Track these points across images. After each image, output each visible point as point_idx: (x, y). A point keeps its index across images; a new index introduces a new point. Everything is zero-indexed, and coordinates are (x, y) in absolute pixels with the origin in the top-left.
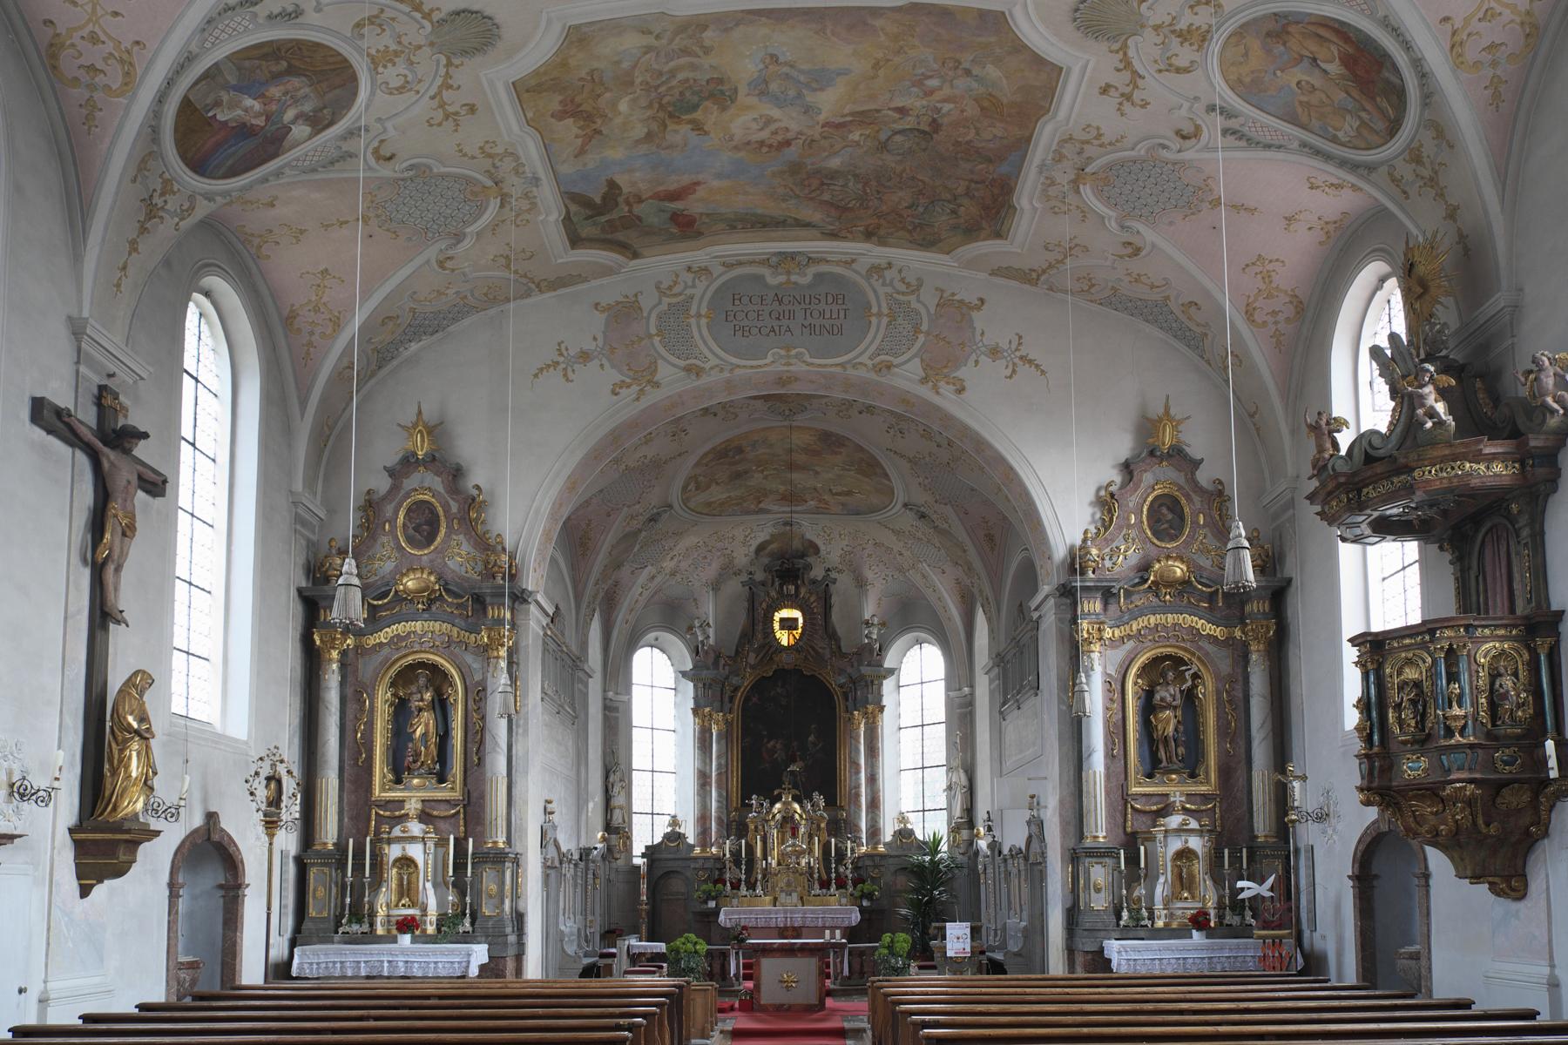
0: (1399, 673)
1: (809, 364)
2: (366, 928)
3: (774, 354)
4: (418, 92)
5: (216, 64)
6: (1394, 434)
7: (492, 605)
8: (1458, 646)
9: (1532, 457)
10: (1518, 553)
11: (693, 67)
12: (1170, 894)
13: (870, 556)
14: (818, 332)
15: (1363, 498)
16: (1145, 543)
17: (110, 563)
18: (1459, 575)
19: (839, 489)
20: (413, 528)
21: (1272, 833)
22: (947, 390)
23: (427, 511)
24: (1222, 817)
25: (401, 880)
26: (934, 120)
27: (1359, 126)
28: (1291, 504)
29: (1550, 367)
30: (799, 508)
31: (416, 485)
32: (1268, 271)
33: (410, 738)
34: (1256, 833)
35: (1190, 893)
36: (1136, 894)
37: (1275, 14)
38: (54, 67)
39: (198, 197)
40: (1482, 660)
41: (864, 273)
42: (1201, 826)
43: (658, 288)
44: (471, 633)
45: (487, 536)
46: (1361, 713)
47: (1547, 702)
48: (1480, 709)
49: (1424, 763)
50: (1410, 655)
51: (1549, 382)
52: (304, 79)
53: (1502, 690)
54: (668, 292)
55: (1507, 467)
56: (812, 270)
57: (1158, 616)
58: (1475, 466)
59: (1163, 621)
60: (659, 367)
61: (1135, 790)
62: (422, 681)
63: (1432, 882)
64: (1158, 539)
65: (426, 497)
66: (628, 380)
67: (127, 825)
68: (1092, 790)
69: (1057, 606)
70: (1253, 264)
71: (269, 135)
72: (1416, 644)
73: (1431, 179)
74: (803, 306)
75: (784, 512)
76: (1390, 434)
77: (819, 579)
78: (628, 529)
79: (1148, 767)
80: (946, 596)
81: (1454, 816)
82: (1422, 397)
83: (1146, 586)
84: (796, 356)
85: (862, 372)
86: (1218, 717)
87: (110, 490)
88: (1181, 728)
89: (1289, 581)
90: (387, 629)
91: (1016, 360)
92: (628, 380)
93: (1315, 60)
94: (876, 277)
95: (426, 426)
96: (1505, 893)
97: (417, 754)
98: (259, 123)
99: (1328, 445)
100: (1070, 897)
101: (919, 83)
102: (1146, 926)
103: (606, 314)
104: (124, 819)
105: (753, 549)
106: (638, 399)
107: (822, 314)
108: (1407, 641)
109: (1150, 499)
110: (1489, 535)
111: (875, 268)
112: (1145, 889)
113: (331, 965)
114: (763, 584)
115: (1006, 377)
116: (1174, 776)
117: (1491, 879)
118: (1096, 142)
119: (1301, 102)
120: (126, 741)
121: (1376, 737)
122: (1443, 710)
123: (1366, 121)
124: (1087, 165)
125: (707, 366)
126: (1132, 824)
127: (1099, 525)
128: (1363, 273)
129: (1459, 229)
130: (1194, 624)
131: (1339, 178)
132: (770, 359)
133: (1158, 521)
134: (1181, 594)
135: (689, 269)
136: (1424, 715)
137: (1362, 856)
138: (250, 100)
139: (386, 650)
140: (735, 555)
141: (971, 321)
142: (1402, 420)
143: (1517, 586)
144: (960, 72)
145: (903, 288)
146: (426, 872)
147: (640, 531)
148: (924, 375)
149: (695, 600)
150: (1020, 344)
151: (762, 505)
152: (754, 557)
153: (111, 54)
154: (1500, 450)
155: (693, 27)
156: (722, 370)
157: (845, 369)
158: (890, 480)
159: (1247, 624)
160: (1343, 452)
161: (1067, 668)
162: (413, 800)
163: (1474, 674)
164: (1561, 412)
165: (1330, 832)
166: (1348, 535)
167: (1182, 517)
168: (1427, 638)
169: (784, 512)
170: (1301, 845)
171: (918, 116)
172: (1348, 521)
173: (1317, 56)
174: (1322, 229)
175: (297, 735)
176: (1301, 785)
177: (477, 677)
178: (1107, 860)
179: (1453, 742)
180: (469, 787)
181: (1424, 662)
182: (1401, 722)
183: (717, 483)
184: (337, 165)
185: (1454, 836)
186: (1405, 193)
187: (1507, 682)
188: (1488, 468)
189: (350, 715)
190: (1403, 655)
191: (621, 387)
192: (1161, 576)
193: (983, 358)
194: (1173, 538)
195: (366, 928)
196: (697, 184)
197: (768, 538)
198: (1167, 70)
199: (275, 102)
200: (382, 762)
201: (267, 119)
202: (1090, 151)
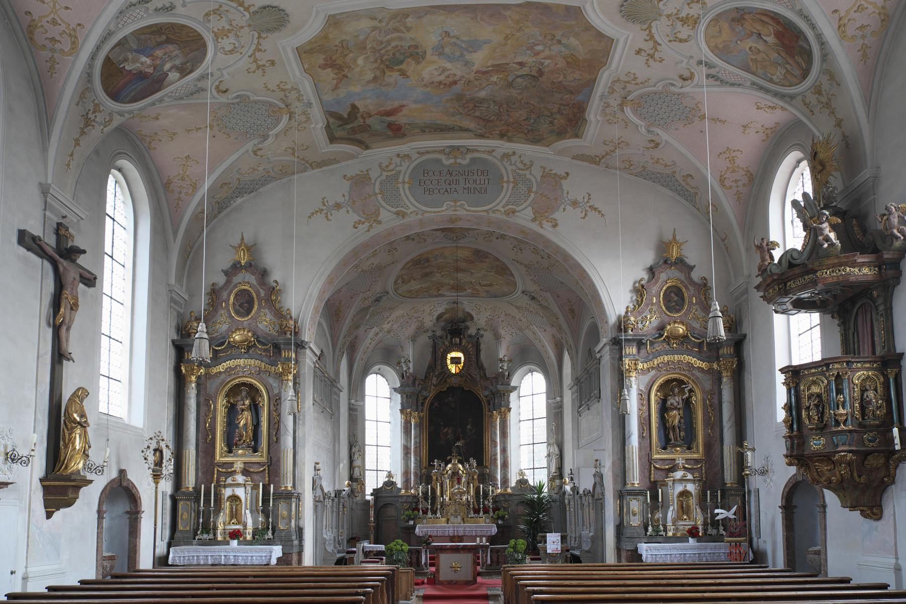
0: (809, 389)
1: (467, 211)
2: (211, 536)
3: (447, 205)
4: (241, 53)
5: (125, 37)
6: (805, 251)
7: (285, 350)
8: (842, 373)
9: (885, 264)
10: (877, 320)
11: (401, 39)
12: (676, 517)
13: (503, 321)
14: (472, 192)
15: (788, 288)
16: (661, 314)
17: (63, 325)
18: (843, 332)
19: (485, 283)
20: (239, 305)
21: (735, 482)
22: (547, 225)
23: (247, 296)
24: (706, 472)
25: (231, 508)
26: (540, 70)
27: (785, 73)
28: (746, 291)
29: (895, 212)
30: (462, 294)
31: (240, 281)
32: (733, 157)
33: (237, 426)
34: (726, 481)
35: (688, 516)
36: (656, 517)
37: (737, 8)
38: (31, 39)
39: (114, 114)
40: (857, 382)
41: (499, 158)
42: (694, 477)
43: (380, 166)
44: (272, 366)
45: (282, 310)
46: (786, 412)
47: (894, 406)
48: (855, 410)
49: (823, 441)
50: (815, 379)
52: (175, 45)
53: (868, 399)
54: (386, 169)
55: (871, 270)
56: (469, 156)
57: (669, 356)
58: (852, 269)
59: (672, 359)
60: (381, 212)
61: (656, 456)
62: (244, 394)
63: (827, 510)
64: (669, 311)
65: (246, 288)
66: (363, 220)
67: (73, 477)
68: (631, 457)
69: (611, 350)
70: (724, 152)
71: (155, 78)
72: (818, 372)
73: (827, 104)
74: (464, 177)
75: (453, 296)
76: (803, 251)
77: (473, 335)
78: (363, 306)
79: (663, 443)
80: (547, 344)
81: (840, 472)
82: (822, 229)
83: (662, 339)
84: (460, 206)
85: (498, 215)
86: (704, 415)
87: (63, 283)
88: (682, 421)
89: (745, 336)
90: (224, 364)
91: (587, 208)
92: (363, 220)
93: (760, 34)
94: (506, 160)
95: (246, 246)
96: (869, 516)
97: (241, 436)
98: (149, 71)
99: (768, 257)
100: (618, 518)
101: (531, 48)
102: (662, 535)
103: (350, 181)
104: (72, 473)
105: (435, 317)
106: (368, 231)
107: (475, 181)
108: (813, 371)
109: (664, 288)
110: (861, 309)
111: (506, 155)
112: (662, 514)
113: (191, 558)
114: (441, 337)
115: (581, 218)
116: (678, 449)
117: (861, 508)
118: (633, 82)
119: (752, 59)
120: (73, 428)
121: (795, 426)
122: (834, 410)
123: (789, 70)
124: (628, 95)
125: (409, 212)
126: (654, 476)
127: (635, 303)
128: (787, 158)
129: (843, 132)
130: (690, 361)
131: (774, 103)
132: (445, 207)
133: (669, 301)
134: (682, 343)
135: (398, 155)
136: (823, 413)
137: (787, 495)
138: (145, 58)
139: (223, 376)
140: (424, 321)
141: (561, 186)
142: (810, 243)
143: (876, 338)
144: (554, 42)
145: (522, 166)
146: (246, 504)
147: (370, 307)
148: (534, 217)
149: (402, 347)
150: (589, 199)
151: (440, 292)
152: (435, 322)
153: (64, 31)
154: (867, 260)
155: (401, 16)
156: (417, 214)
157: (488, 213)
158: (514, 277)
159: (720, 361)
160: (776, 261)
161: (617, 386)
162: (239, 462)
163: (852, 389)
164: (902, 238)
165: (768, 481)
166: (779, 309)
167: (683, 299)
168: (825, 369)
169: (453, 296)
170: (752, 489)
171: (530, 67)
172: (779, 301)
173: (761, 32)
174: (764, 132)
175: (172, 425)
176: (752, 454)
177: (276, 391)
178: (640, 497)
179: (839, 429)
180: (271, 455)
181: (823, 383)
182: (809, 417)
183: (414, 279)
184: (195, 95)
185: (840, 483)
186: (812, 111)
187: (871, 394)
188: (860, 270)
189: (202, 413)
190: (811, 378)
191: (359, 224)
192: (671, 333)
193: (568, 207)
194: (678, 311)
195: (211, 536)
196: (403, 106)
197: (444, 311)
198: (674, 41)
199: (159, 59)
200: (221, 441)
201: (154, 69)
202: (630, 87)
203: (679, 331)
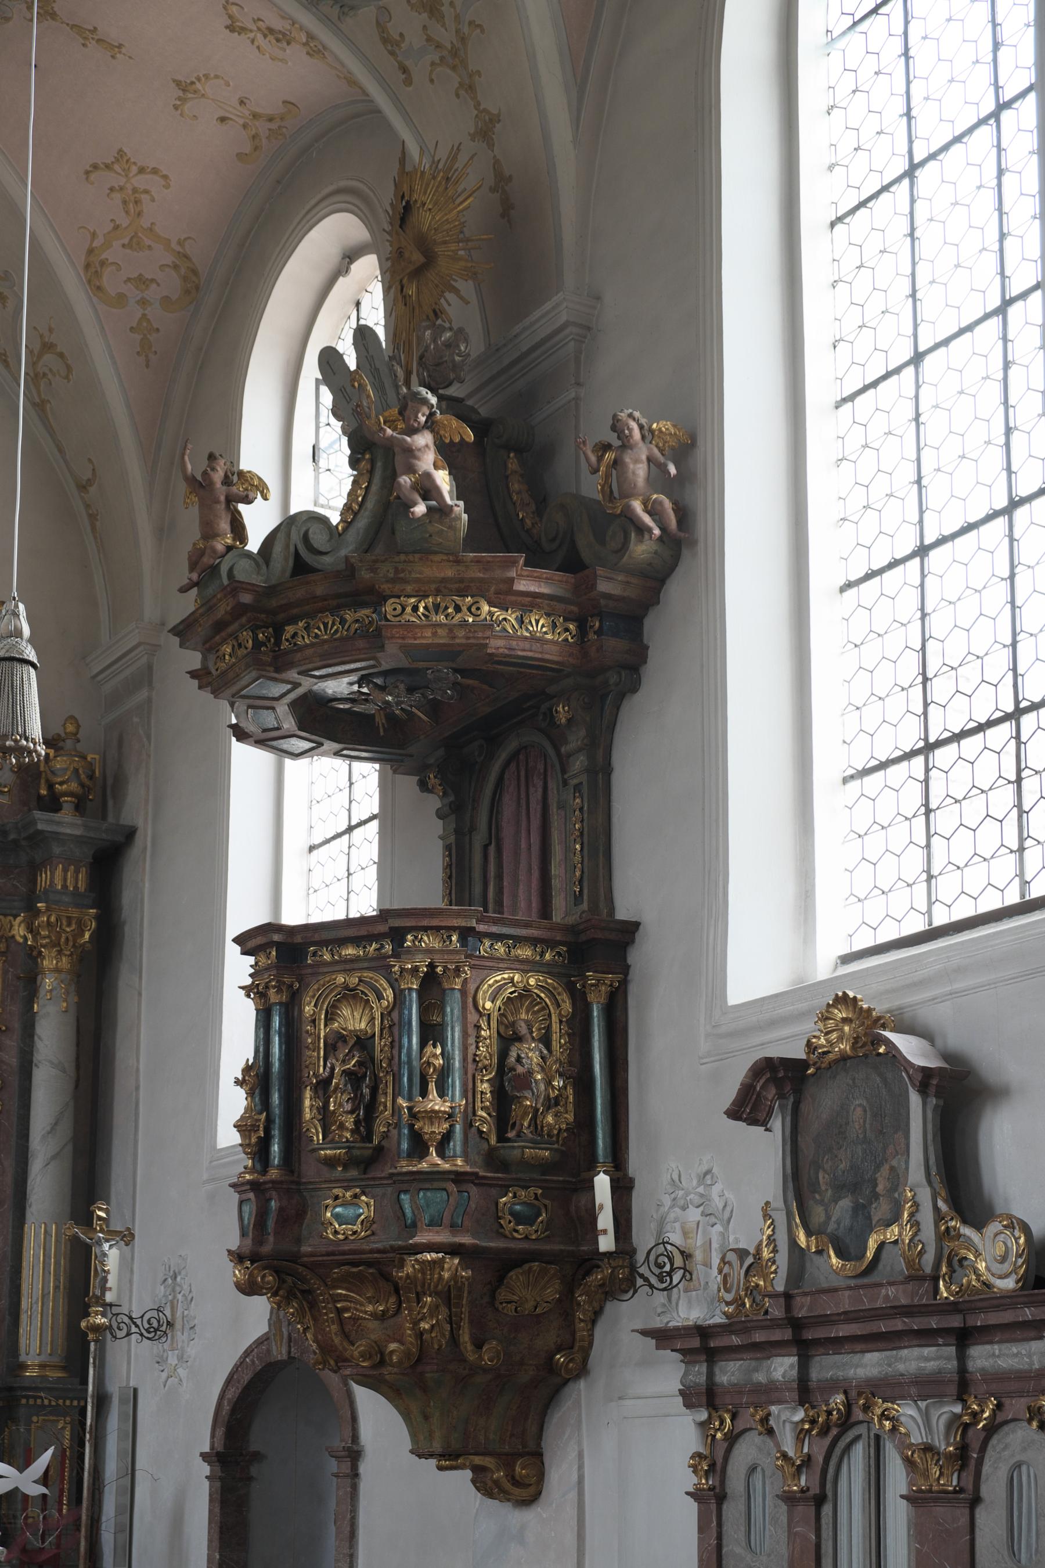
0: (330, 1018)
6: (352, 531)
8: (445, 969)
9: (600, 615)
10: (562, 806)
15: (285, 645)
18: (452, 839)
21: (56, 1360)
28: (146, 677)
29: (641, 444)
32: (135, 190)
34: (23, 1358)
40: (488, 1005)
46: (250, 1094)
47: (599, 1101)
48: (478, 1104)
49: (366, 1208)
50: (354, 981)
51: (639, 471)
53: (520, 1070)
55: (554, 626)
58: (499, 614)
63: (363, 1468)
70: (108, 167)
72: (365, 958)
73: (454, 53)
76: (345, 530)
81: (416, 1323)
82: (410, 452)
89: (130, 834)
96: (502, 1490)
99: (224, 525)
108: (350, 951)
110: (513, 766)
117: (478, 1460)
121: (275, 1148)
122: (410, 1099)
128: (314, 234)
129: (497, 162)
131: (284, 16)
136: (371, 1108)
137: (233, 1411)
142: (370, 505)
143: (556, 870)
154: (545, 589)
159: (38, 913)
160: (253, 545)
163: (471, 1031)
164: (657, 532)
165: (173, 1360)
166: (250, 727)
168: (388, 948)
170: (113, 1388)
172: (253, 689)
174: (245, 126)
176: (122, 1257)
179: (424, 1166)
181: (380, 997)
182: (326, 1117)
185: (413, 1367)
186: (404, 70)
187: (531, 1053)
188: (521, 622)
190: (341, 979)
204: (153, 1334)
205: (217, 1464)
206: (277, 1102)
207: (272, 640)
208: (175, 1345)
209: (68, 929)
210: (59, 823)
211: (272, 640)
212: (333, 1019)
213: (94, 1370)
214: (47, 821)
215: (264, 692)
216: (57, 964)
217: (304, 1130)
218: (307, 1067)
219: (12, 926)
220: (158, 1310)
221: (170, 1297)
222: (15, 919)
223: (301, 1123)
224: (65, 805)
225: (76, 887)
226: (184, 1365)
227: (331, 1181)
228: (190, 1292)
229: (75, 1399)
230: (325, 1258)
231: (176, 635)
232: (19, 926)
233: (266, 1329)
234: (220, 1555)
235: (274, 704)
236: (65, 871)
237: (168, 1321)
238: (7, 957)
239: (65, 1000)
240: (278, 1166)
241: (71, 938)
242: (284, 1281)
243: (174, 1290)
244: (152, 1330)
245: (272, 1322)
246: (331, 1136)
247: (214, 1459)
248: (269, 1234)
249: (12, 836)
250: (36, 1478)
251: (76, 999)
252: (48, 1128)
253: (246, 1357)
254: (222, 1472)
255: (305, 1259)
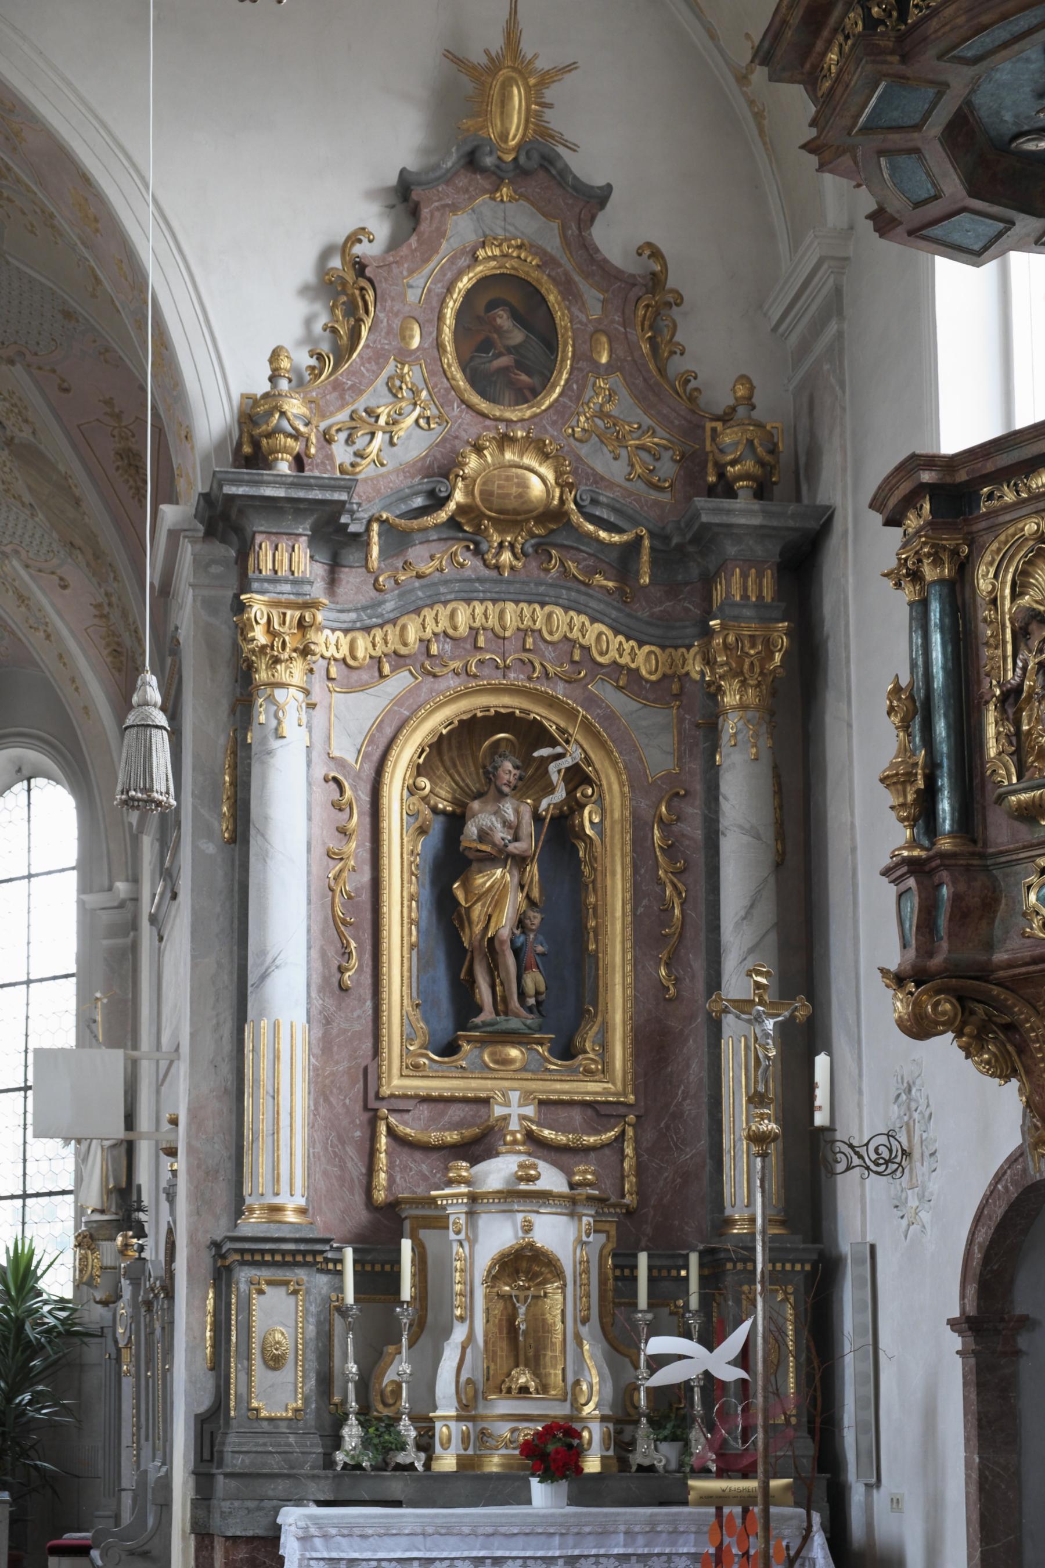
12: (480, 1378)
16: (446, 403)
24: (640, 1169)
34: (728, 1211)
35: (537, 1374)
36: (390, 1376)
42: (572, 1186)
57: (479, 609)
59: (492, 621)
61: (396, 1083)
64: (483, 395)
68: (265, 1074)
69: (200, 564)
79: (445, 1024)
83: (443, 516)
86: (637, 893)
88: (535, 919)
100: (209, 1382)
102: (411, 1467)
109: (464, 283)
112: (409, 1361)
116: (514, 1053)
121: (945, 805)
126: (391, 1179)
127: (325, 348)
130: (575, 634)
133: (486, 346)
134: (541, 549)
137: (986, 1260)
161: (222, 740)
165: (913, 1202)
167: (550, 343)
178: (301, 1274)
192: (486, 495)
194: (526, 395)
203: (524, 485)
204: (884, 1167)
205: (969, 1333)
206: (944, 734)
207: (895, 14)
208: (914, 1181)
209: (752, 652)
210: (729, 512)
211: (895, 14)
212: (1022, 594)
213: (763, 1196)
214: (714, 510)
215: (896, 114)
216: (741, 698)
217: (989, 773)
218: (988, 675)
219: (685, 660)
220: (888, 1135)
221: (906, 1118)
222: (688, 650)
223: (983, 766)
224: (740, 493)
225: (760, 597)
226: (927, 1205)
227: (1031, 846)
228: (928, 1106)
229: (798, 1261)
230: (1031, 968)
231: (811, 152)
232: (694, 660)
233: (1020, 1141)
234: (980, 1458)
235: (915, 139)
236: (744, 576)
237: (903, 1150)
238: (681, 701)
239: (755, 745)
240: (950, 832)
241: (757, 663)
242: (972, 1013)
243: (909, 1108)
244: (881, 1161)
245: (1026, 1128)
246: (1028, 774)
247: (965, 1326)
248: (942, 939)
249: (675, 540)
250: (732, 1358)
251: (769, 743)
252: (742, 913)
253: (997, 1183)
254: (977, 1343)
255: (1002, 974)
